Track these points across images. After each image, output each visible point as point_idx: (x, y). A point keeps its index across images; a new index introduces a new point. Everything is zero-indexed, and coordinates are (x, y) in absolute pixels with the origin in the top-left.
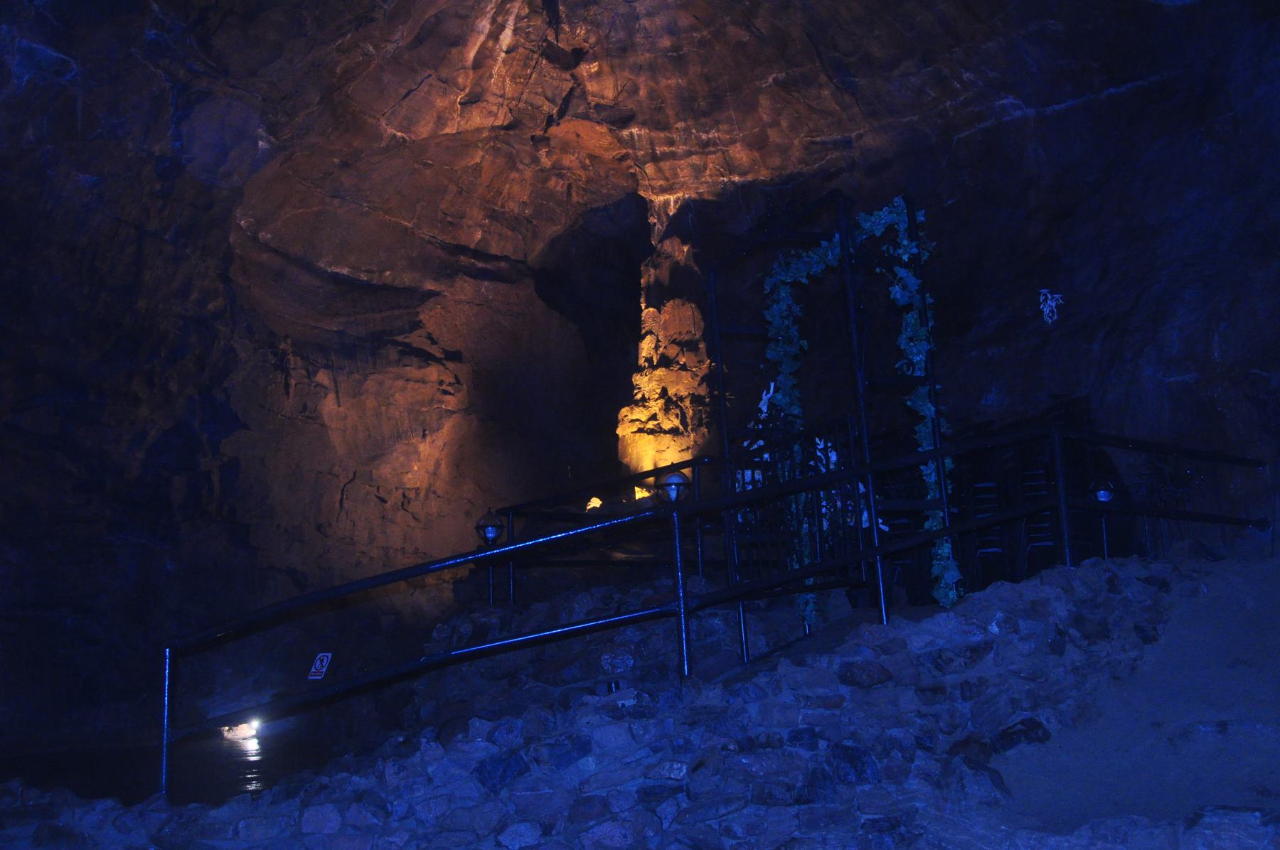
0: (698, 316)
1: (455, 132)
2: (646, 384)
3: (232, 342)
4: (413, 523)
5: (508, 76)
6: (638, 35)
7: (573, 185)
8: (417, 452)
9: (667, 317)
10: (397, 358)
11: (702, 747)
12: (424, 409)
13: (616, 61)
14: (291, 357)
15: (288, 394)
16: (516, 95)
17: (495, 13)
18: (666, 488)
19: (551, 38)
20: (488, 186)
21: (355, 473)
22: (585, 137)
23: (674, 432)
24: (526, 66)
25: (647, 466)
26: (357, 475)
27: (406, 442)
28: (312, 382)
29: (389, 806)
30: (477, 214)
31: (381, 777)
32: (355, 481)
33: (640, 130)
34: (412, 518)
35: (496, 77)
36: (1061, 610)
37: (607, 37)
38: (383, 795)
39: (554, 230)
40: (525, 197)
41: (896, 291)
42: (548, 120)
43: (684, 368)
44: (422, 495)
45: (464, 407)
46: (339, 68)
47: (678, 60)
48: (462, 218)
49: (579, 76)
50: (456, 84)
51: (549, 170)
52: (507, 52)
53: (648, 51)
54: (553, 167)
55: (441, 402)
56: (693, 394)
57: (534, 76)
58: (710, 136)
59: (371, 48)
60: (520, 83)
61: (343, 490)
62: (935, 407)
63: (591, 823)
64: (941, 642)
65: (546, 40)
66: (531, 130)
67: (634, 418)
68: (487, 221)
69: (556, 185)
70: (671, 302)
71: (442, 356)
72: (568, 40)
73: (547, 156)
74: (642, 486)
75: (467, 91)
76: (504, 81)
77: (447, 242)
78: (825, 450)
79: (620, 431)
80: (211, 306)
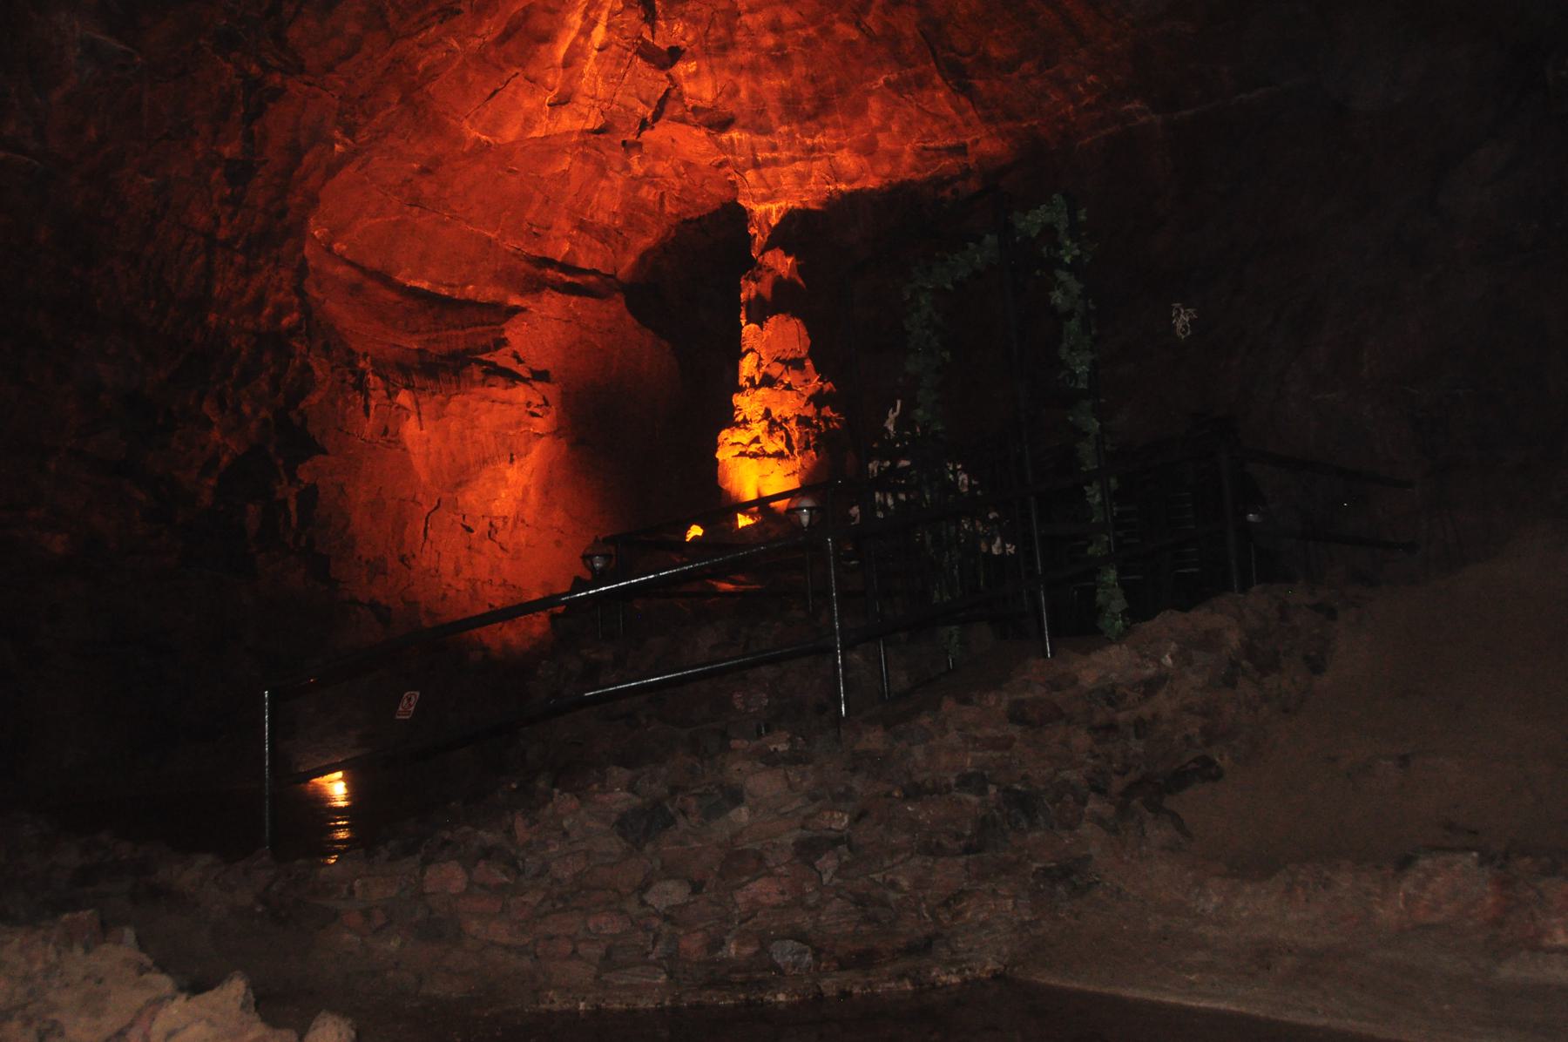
0: (804, 332)
1: (543, 135)
2: (748, 404)
3: (309, 360)
4: (500, 554)
5: (601, 75)
6: (739, 33)
7: (665, 194)
8: (505, 479)
9: (770, 333)
10: (482, 378)
11: (865, 795)
12: (511, 433)
13: (716, 60)
14: (370, 376)
15: (368, 415)
16: (608, 96)
17: (587, 7)
18: (797, 512)
19: (647, 36)
20: (576, 195)
21: (439, 501)
22: (681, 143)
23: (779, 455)
24: (619, 65)
25: (751, 495)
26: (441, 504)
27: (492, 467)
28: (393, 403)
29: (520, 863)
30: (564, 225)
31: (510, 831)
32: (440, 509)
33: (741, 135)
34: (499, 548)
35: (587, 76)
36: (1234, 639)
37: (706, 34)
38: (513, 851)
39: (645, 242)
40: (616, 207)
41: (1057, 297)
42: (641, 124)
43: (789, 387)
44: (510, 523)
45: (552, 430)
46: (421, 66)
47: (780, 59)
48: (548, 228)
49: (676, 76)
50: (545, 85)
51: (642, 177)
52: (599, 50)
53: (749, 49)
54: (646, 175)
55: (530, 425)
56: (799, 416)
57: (627, 75)
58: (815, 141)
59: (455, 44)
60: (613, 83)
61: (427, 519)
62: (1100, 422)
63: (745, 879)
64: (1114, 675)
65: (640, 37)
66: (624, 135)
67: (735, 441)
68: (575, 232)
69: (647, 193)
70: (775, 317)
71: (529, 376)
72: (664, 37)
73: (639, 163)
74: (744, 513)
75: (556, 91)
76: (596, 80)
77: (533, 254)
78: (954, 472)
79: (719, 455)
80: (285, 322)
